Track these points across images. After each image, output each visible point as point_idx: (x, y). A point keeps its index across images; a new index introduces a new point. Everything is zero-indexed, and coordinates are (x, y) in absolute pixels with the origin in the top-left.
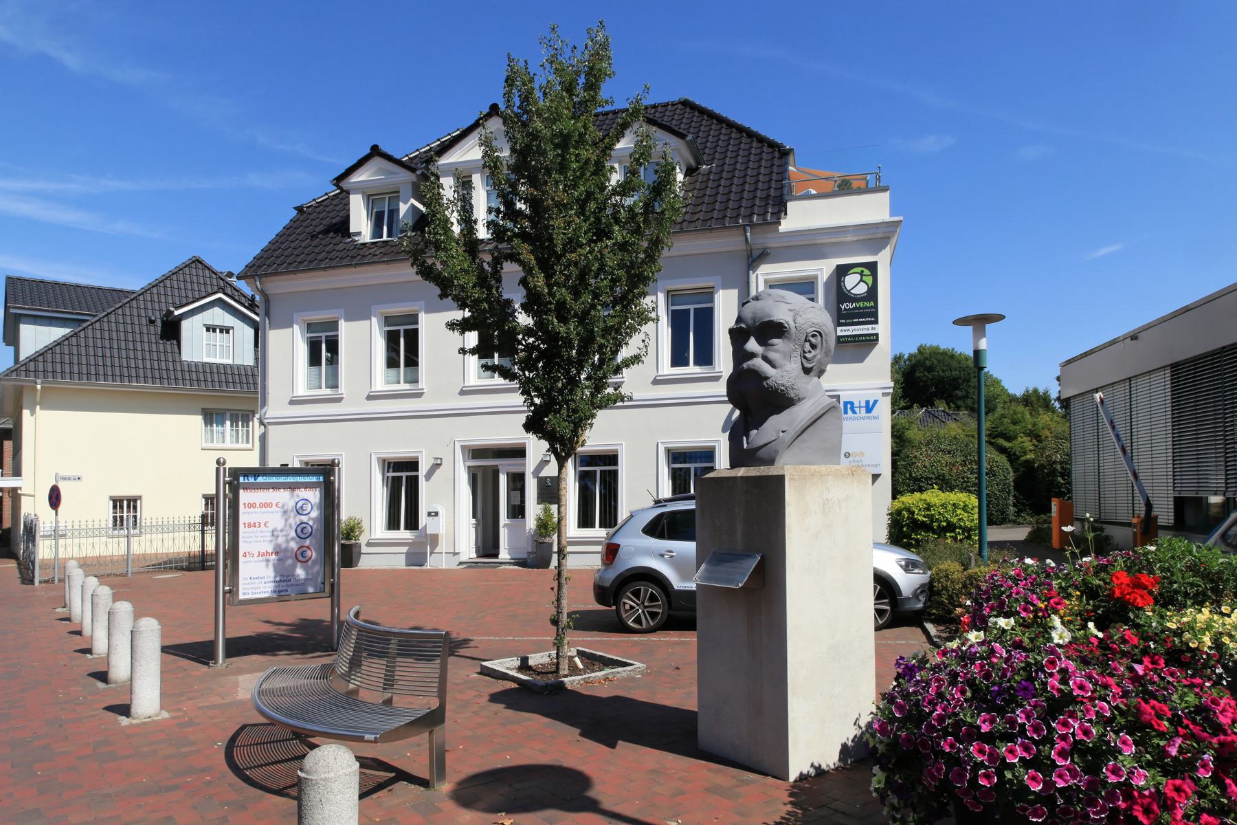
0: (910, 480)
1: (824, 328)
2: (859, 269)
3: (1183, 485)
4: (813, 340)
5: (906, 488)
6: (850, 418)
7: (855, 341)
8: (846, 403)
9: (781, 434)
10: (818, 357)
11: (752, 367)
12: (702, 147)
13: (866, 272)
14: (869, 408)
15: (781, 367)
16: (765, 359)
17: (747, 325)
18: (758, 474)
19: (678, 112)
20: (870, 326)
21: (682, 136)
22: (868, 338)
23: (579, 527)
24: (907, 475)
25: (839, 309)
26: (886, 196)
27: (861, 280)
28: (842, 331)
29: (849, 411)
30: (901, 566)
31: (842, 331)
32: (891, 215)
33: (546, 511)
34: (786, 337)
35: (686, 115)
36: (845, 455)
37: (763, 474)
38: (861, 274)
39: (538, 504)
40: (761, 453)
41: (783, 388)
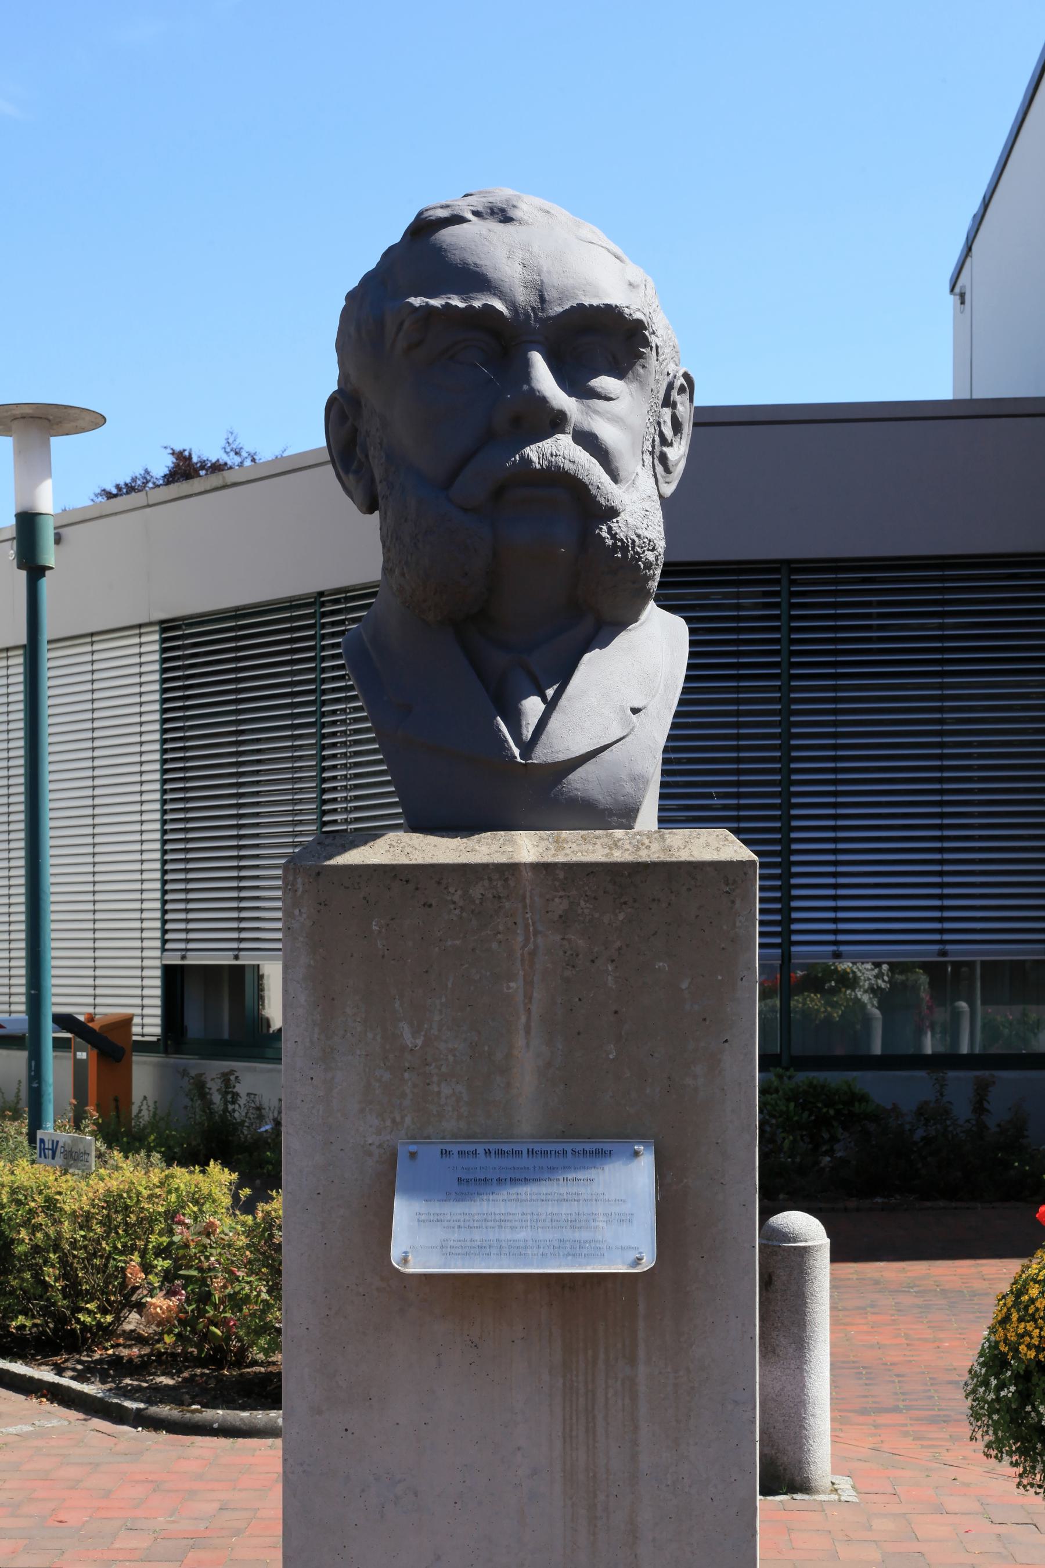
3: (191, 936)
16: (588, 440)
34: (637, 378)
40: (580, 781)
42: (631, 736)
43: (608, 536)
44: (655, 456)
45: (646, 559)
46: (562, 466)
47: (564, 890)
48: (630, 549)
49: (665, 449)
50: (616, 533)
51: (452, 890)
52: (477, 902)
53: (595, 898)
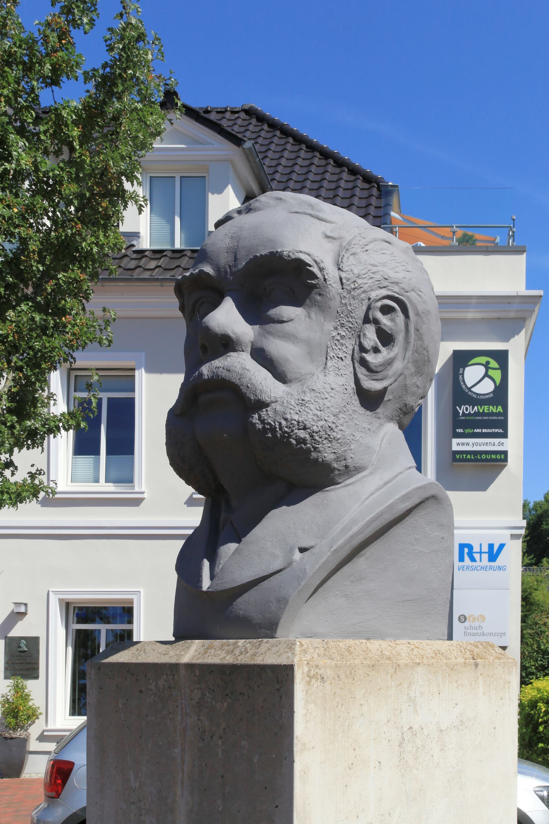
0: (538, 653)
1: (412, 295)
2: (483, 359)
4: (385, 320)
5: (533, 663)
6: (468, 568)
7: (476, 460)
8: (462, 546)
9: (297, 555)
10: (398, 366)
11: (224, 374)
12: (271, 171)
13: (493, 364)
14: (493, 554)
15: (300, 380)
17: (217, 269)
18: (229, 660)
19: (239, 122)
20: (496, 441)
21: (237, 141)
22: (494, 457)
23: (70, 715)
24: (535, 647)
25: (455, 413)
26: (521, 260)
27: (486, 375)
28: (458, 444)
29: (466, 557)
30: (542, 798)
31: (458, 444)
32: (528, 287)
33: (18, 689)
34: (316, 304)
35: (251, 127)
36: (459, 619)
37: (244, 660)
38: (487, 366)
39: (6, 678)
41: (302, 434)
42: (288, 569)
43: (258, 422)
44: (355, 361)
45: (296, 436)
46: (220, 374)
47: (199, 684)
48: (278, 429)
49: (364, 355)
50: (264, 419)
51: (151, 681)
52: (161, 690)
53: (213, 691)
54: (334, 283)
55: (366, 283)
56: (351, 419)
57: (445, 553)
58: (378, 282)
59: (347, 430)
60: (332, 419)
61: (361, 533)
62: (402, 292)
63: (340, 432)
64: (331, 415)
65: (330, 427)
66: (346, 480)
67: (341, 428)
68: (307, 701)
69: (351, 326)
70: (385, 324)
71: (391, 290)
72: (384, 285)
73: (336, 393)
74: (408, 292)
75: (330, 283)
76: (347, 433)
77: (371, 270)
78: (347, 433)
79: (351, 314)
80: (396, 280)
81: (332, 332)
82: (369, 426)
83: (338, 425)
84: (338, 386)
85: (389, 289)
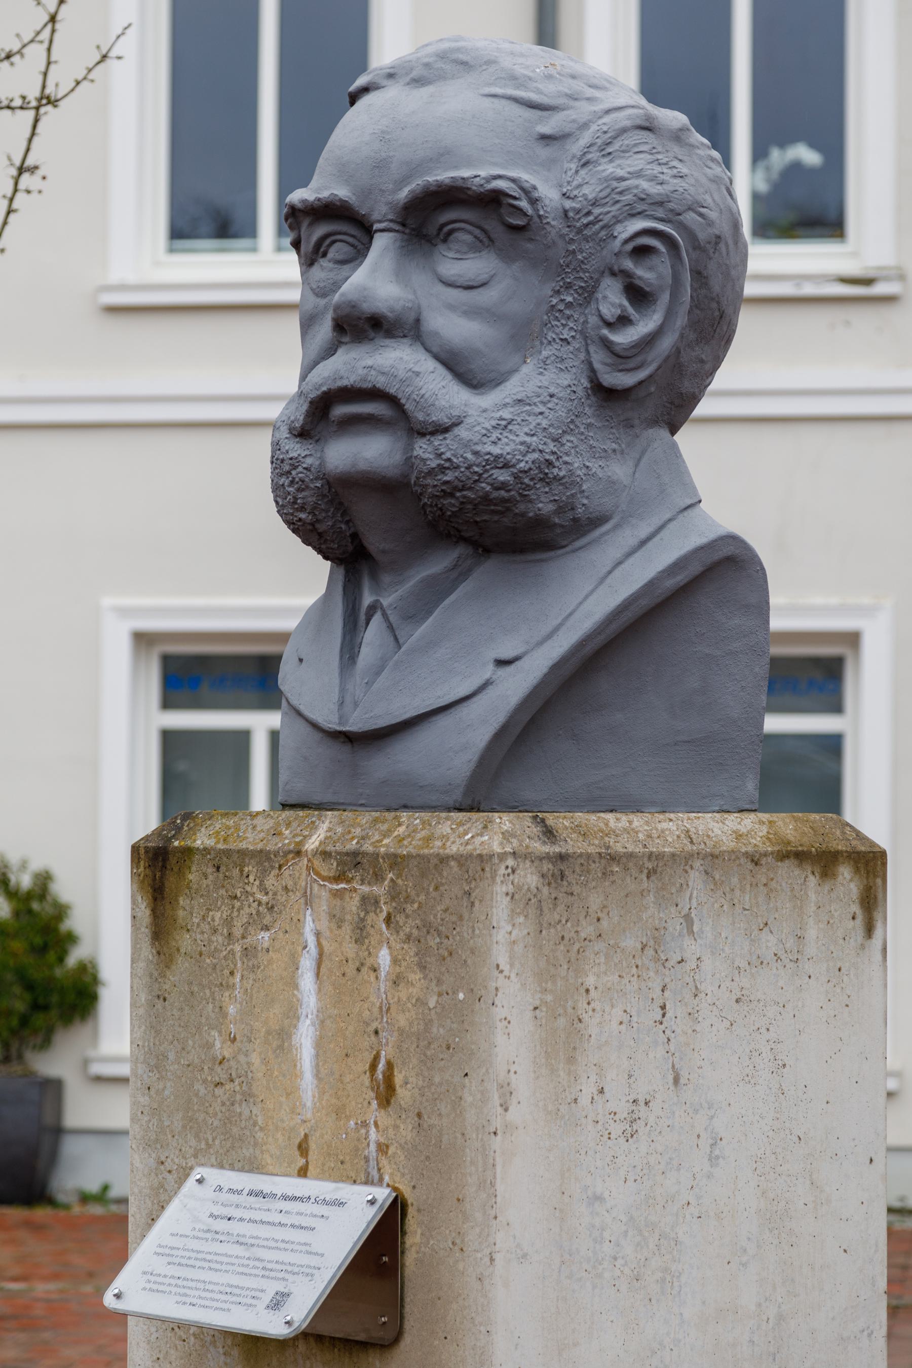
54: (553, 220)
55: (609, 212)
56: (582, 440)
57: (752, 654)
58: (628, 208)
59: (576, 460)
60: (552, 446)
61: (599, 634)
62: (670, 216)
63: (564, 466)
64: (549, 441)
65: (547, 460)
66: (574, 540)
67: (566, 459)
68: (513, 911)
69: (583, 285)
70: (640, 278)
71: (651, 215)
72: (639, 210)
73: (556, 401)
74: (680, 214)
75: (548, 220)
76: (576, 465)
77: (616, 188)
78: (576, 465)
79: (583, 266)
80: (659, 199)
81: (551, 299)
82: (614, 446)
83: (561, 455)
84: (560, 389)
85: (647, 216)
